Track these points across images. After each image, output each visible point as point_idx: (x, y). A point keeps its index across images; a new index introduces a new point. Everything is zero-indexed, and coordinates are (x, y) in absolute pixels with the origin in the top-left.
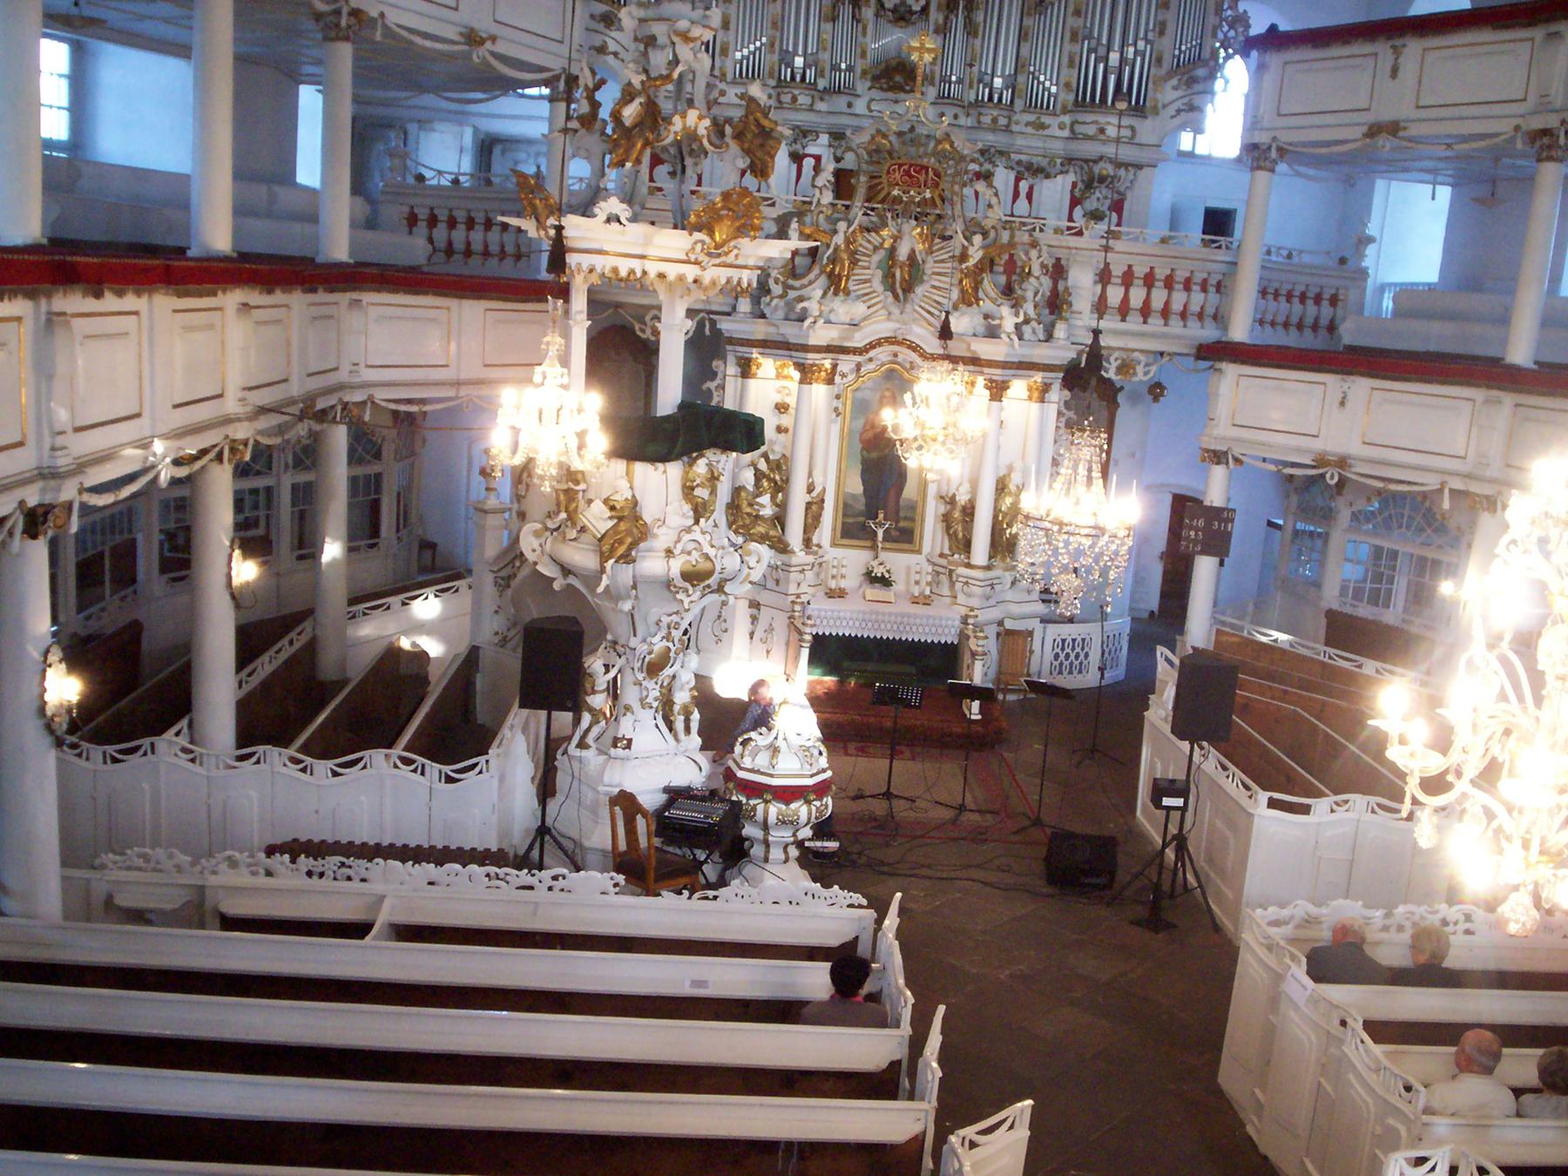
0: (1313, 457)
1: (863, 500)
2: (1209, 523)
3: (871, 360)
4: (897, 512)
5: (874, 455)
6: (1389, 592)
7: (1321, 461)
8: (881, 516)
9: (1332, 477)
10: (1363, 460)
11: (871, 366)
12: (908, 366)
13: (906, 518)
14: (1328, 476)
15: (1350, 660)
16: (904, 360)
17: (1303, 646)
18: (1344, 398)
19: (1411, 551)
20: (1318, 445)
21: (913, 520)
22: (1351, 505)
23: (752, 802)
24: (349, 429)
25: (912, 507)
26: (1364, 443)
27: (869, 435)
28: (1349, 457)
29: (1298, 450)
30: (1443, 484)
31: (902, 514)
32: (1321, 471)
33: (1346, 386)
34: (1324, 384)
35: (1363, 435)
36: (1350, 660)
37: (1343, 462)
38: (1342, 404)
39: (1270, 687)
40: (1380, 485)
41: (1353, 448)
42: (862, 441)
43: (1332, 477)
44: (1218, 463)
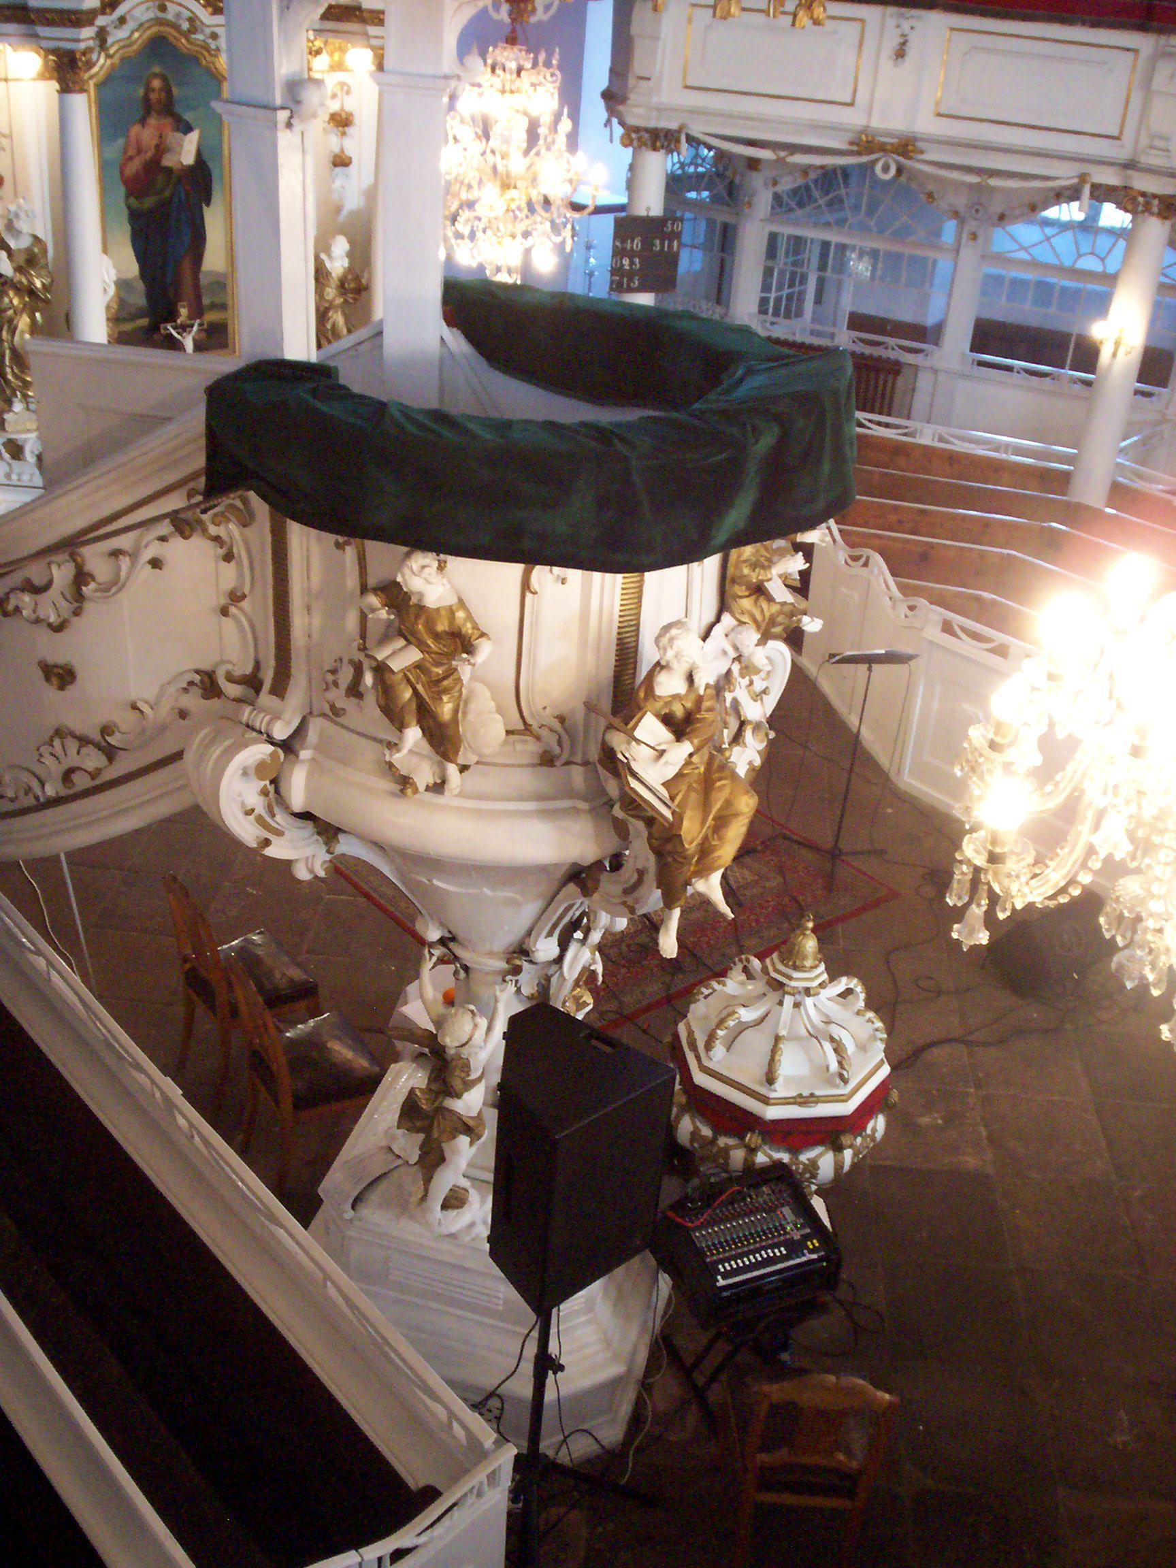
0: (849, 136)
1: (140, 286)
2: (648, 245)
3: (122, 20)
4: (199, 297)
5: (149, 202)
6: (766, 287)
7: (867, 144)
8: (184, 312)
9: (886, 169)
10: (940, 142)
11: (122, 33)
12: (185, 26)
13: (214, 306)
14: (878, 168)
15: (897, 427)
16: (178, 15)
17: (879, 424)
18: (904, 44)
19: (875, 245)
20: (854, 119)
21: (223, 307)
22: (775, 184)
23: (805, 1157)
24: (801, 1153)
25: (222, 284)
26: (940, 115)
27: (134, 167)
28: (916, 139)
29: (816, 127)
30: (1083, 178)
31: (206, 301)
32: (864, 159)
33: (906, 26)
34: (862, 20)
35: (937, 104)
36: (897, 427)
37: (906, 146)
38: (900, 53)
39: (895, 508)
40: (973, 179)
41: (925, 124)
42: (126, 182)
43: (886, 169)
44: (655, 149)
